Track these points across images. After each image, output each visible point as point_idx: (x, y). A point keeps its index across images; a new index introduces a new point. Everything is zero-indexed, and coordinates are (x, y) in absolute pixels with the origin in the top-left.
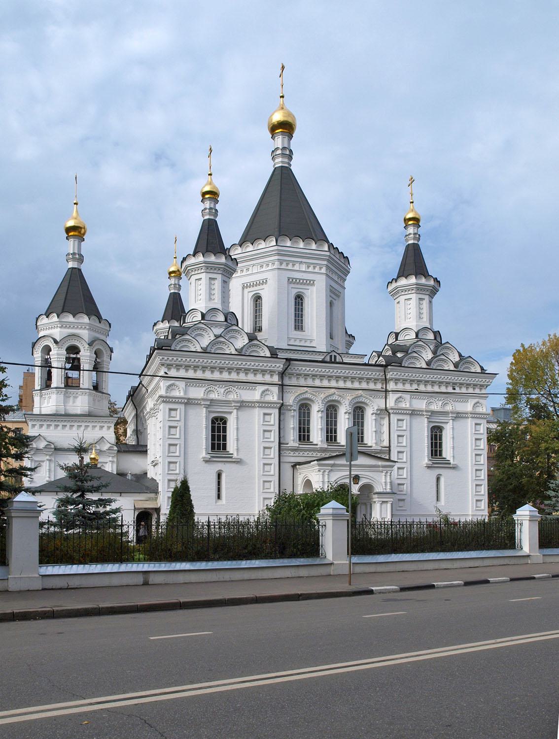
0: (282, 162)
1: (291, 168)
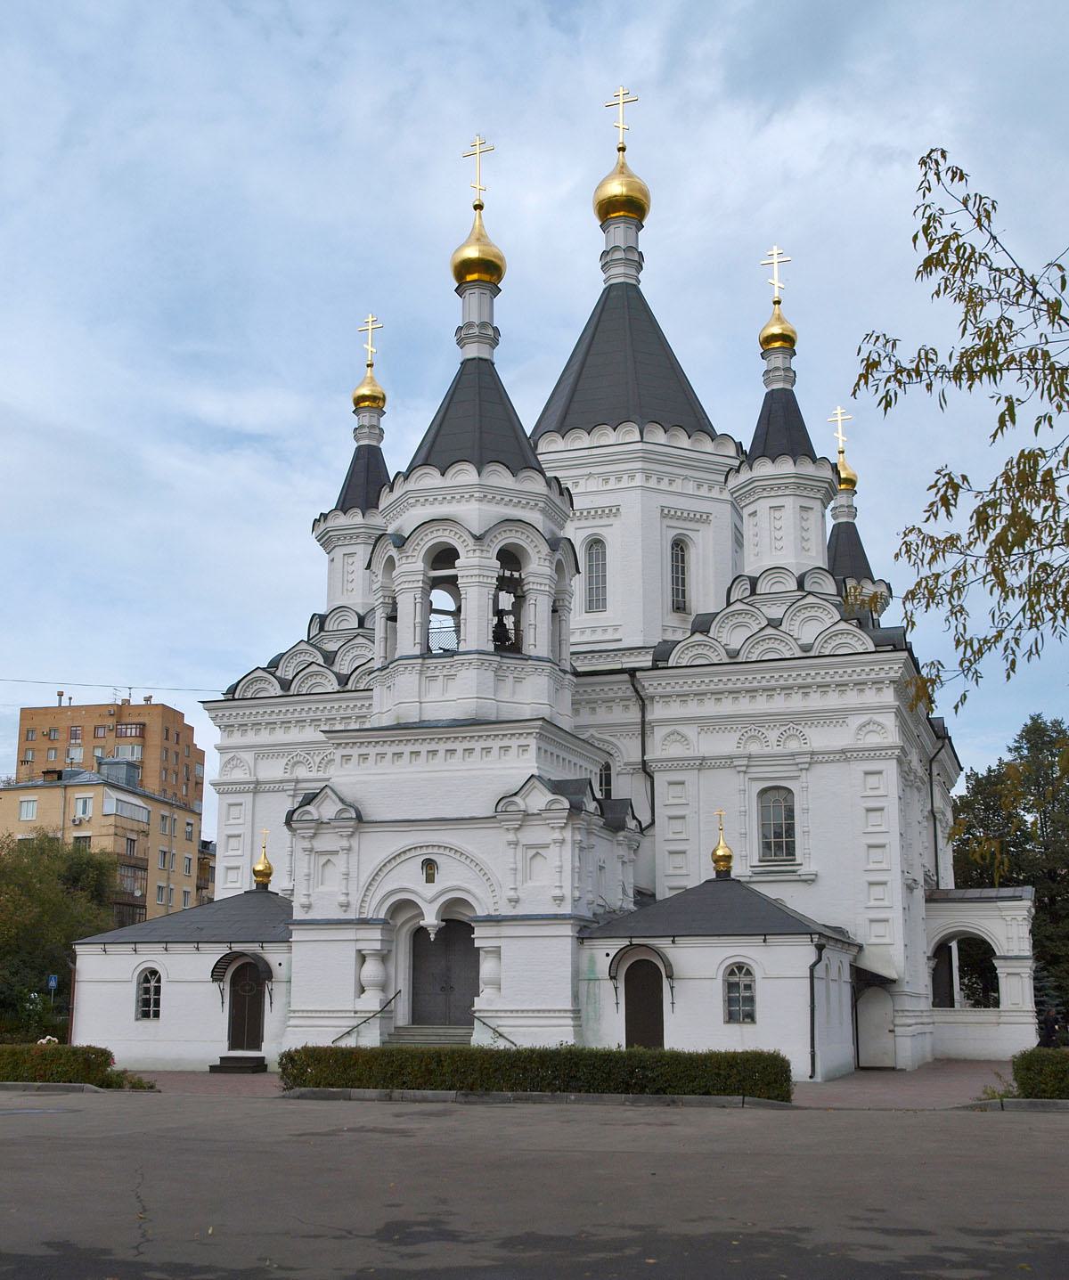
0: (625, 275)
1: (640, 286)
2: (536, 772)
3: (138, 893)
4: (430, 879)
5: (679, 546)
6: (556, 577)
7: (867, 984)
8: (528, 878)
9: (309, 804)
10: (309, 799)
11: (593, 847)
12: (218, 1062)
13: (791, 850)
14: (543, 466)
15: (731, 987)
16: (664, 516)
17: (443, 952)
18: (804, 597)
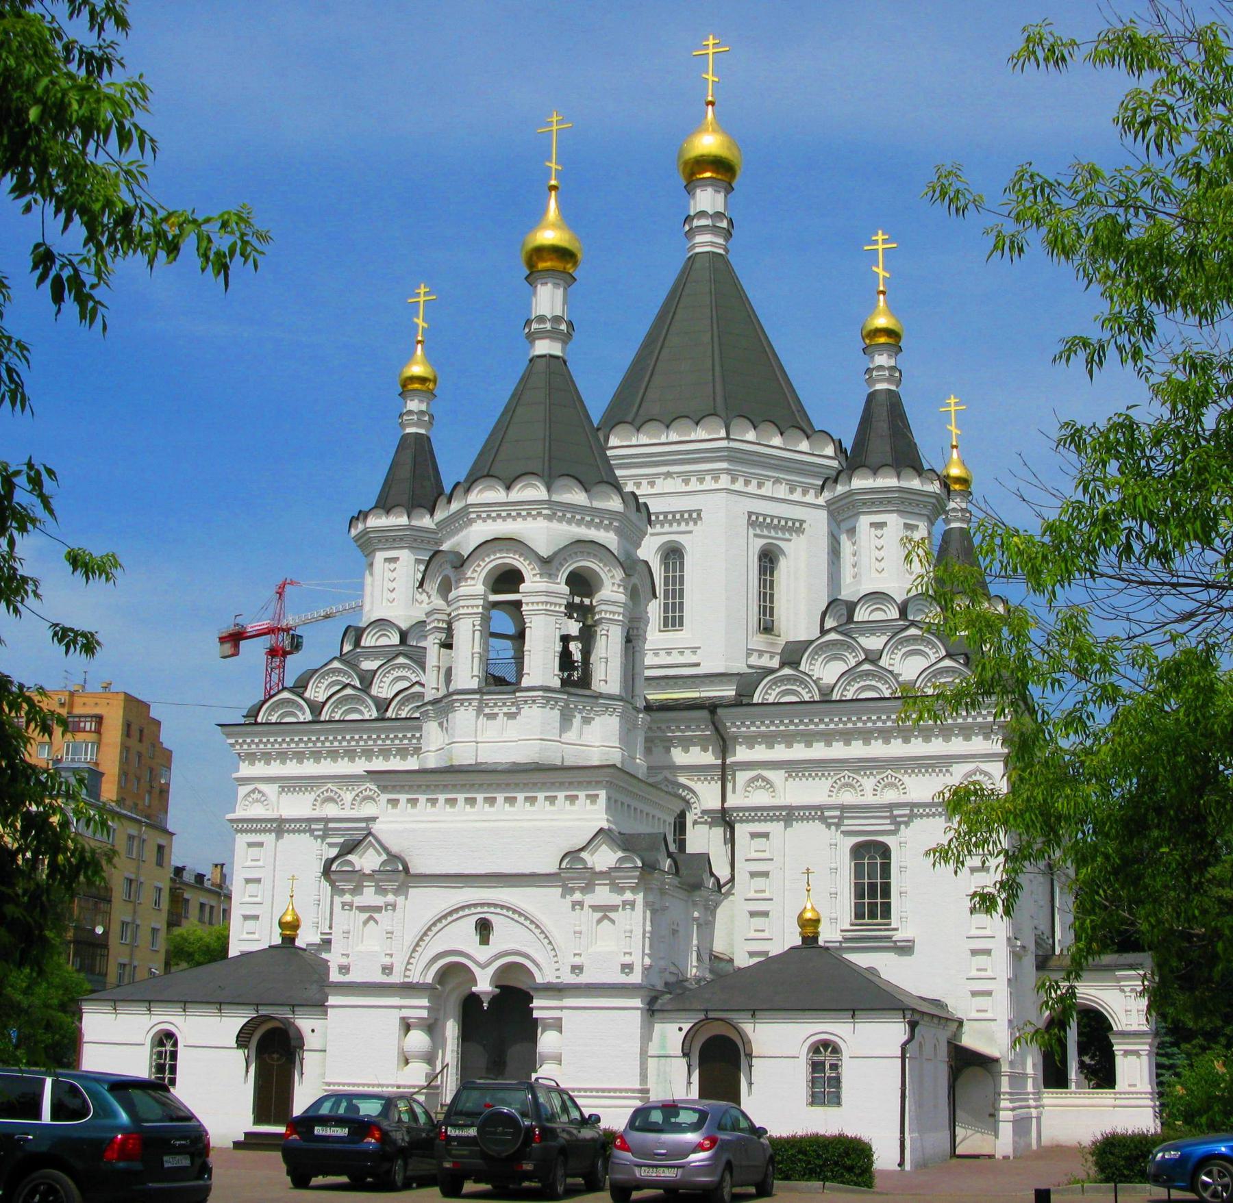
0: (712, 244)
2: (605, 825)
3: (99, 930)
4: (485, 940)
5: (768, 559)
6: (630, 604)
7: (967, 1065)
8: (591, 941)
9: (349, 853)
10: (350, 847)
11: (665, 909)
12: (242, 1138)
13: (887, 913)
14: (618, 473)
15: (816, 1067)
16: (752, 524)
17: (499, 1021)
18: (907, 628)
